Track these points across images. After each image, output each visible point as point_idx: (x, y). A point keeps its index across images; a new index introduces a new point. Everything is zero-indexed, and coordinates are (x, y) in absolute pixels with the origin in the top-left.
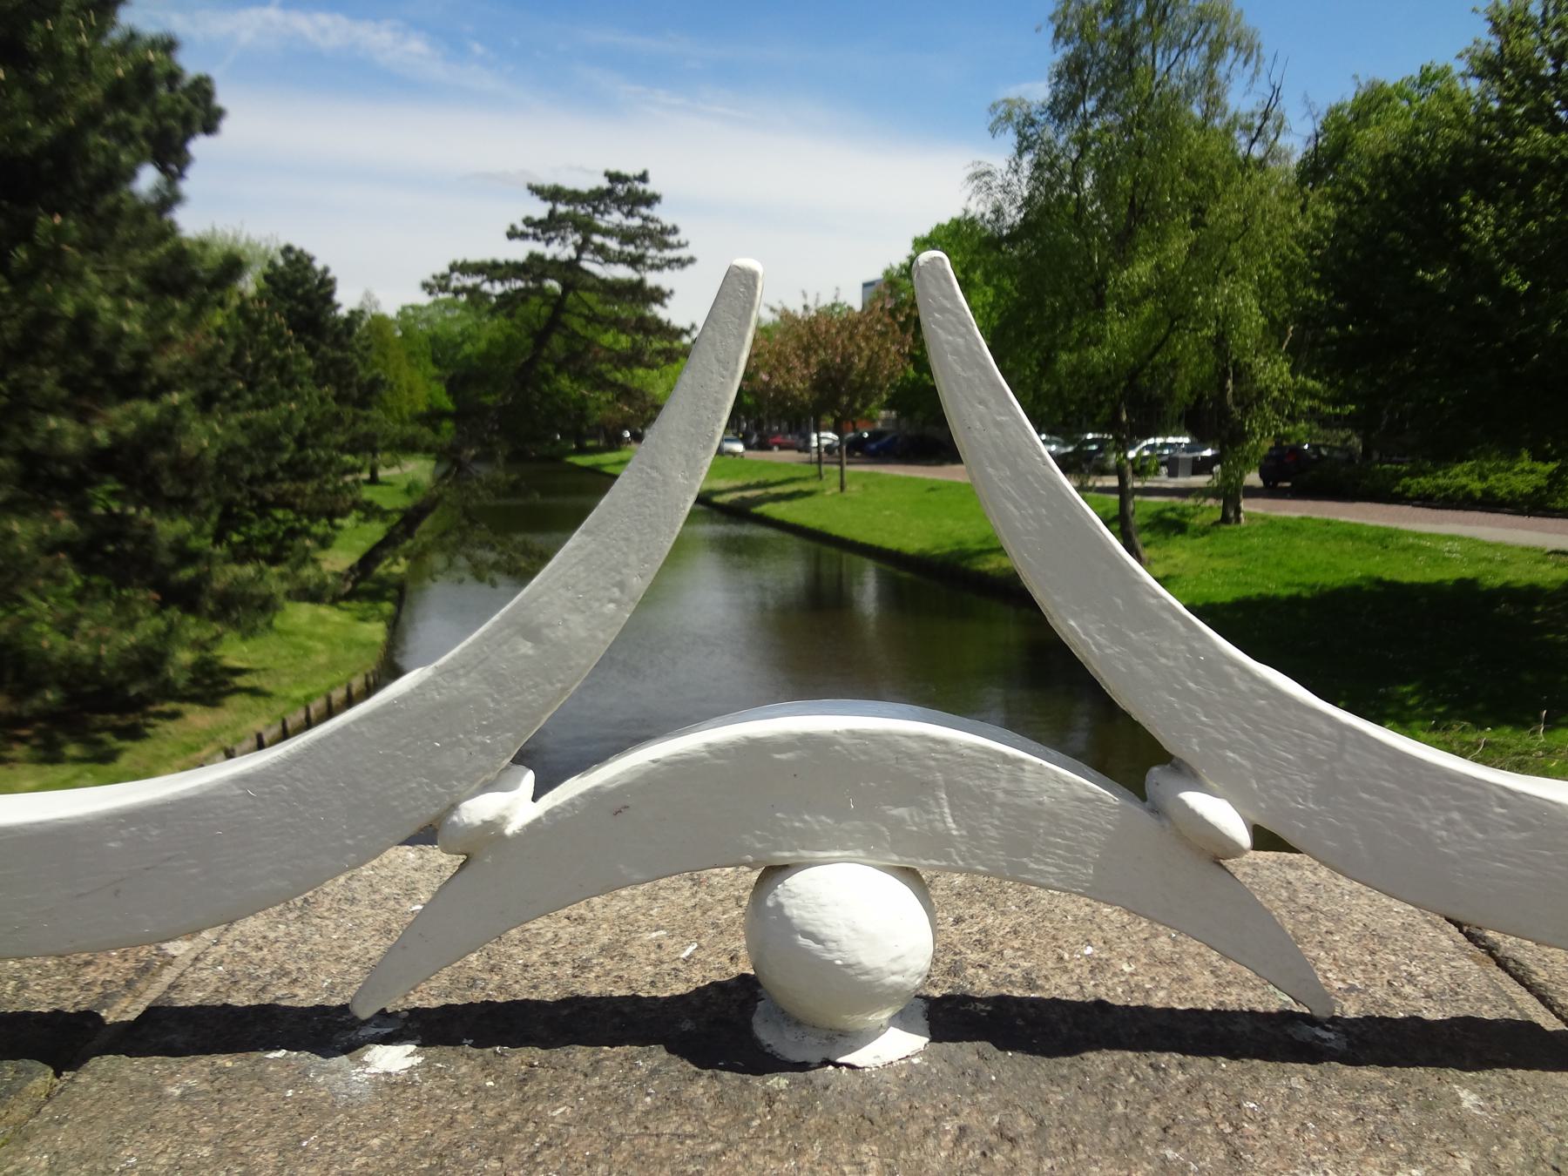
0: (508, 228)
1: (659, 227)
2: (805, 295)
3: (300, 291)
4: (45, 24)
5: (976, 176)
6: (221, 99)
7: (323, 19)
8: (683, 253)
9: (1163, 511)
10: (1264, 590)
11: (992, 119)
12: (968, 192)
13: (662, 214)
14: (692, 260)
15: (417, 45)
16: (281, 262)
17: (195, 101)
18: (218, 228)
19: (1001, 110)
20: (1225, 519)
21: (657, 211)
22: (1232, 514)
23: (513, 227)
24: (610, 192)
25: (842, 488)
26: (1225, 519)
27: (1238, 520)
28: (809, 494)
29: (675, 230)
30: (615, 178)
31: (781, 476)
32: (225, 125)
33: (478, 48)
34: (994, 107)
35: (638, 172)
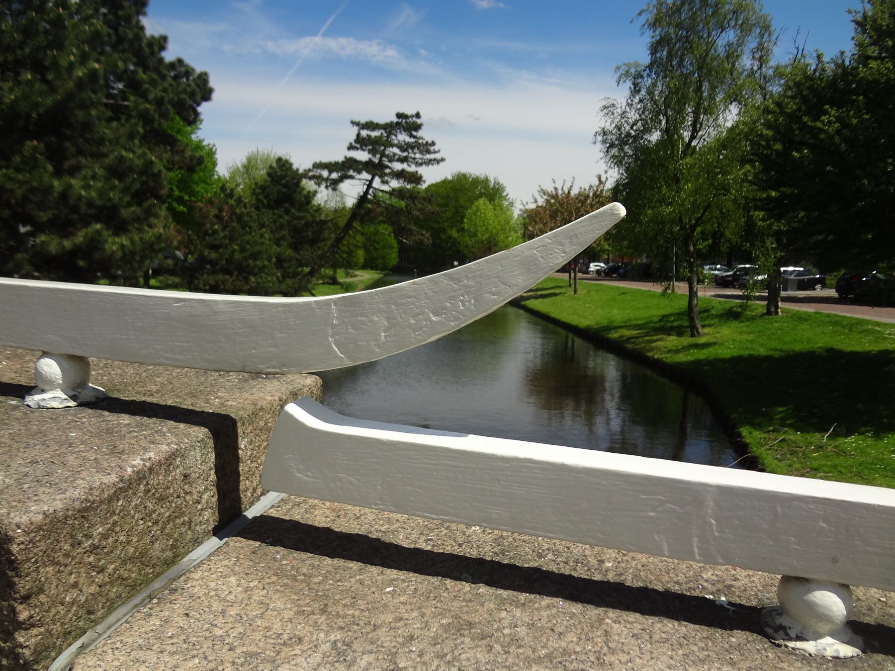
0: (348, 145)
1: (424, 142)
2: (554, 182)
3: (284, 182)
4: (53, 51)
5: (605, 107)
6: (212, 83)
7: (343, 41)
8: (438, 156)
9: (733, 307)
10: (753, 352)
11: (618, 74)
12: (599, 118)
13: (425, 135)
14: (442, 160)
15: (391, 52)
16: (274, 165)
17: (198, 86)
18: (260, 150)
19: (623, 70)
20: (769, 313)
21: (420, 134)
22: (773, 310)
23: (351, 144)
24: (397, 123)
25: (575, 292)
26: (769, 313)
27: (777, 313)
28: (555, 295)
29: (433, 144)
30: (399, 116)
31: (552, 285)
32: (214, 96)
33: (423, 52)
34: (618, 68)
35: (414, 113)
